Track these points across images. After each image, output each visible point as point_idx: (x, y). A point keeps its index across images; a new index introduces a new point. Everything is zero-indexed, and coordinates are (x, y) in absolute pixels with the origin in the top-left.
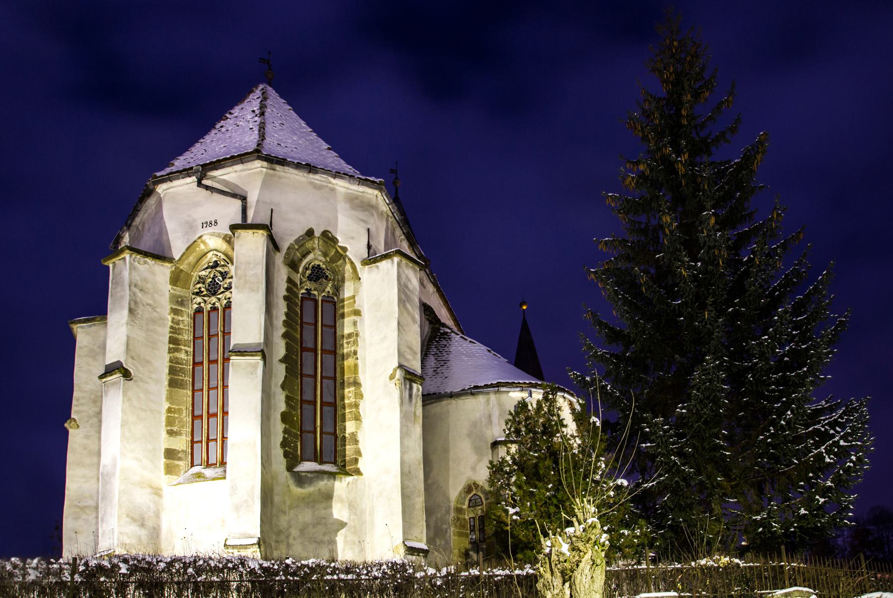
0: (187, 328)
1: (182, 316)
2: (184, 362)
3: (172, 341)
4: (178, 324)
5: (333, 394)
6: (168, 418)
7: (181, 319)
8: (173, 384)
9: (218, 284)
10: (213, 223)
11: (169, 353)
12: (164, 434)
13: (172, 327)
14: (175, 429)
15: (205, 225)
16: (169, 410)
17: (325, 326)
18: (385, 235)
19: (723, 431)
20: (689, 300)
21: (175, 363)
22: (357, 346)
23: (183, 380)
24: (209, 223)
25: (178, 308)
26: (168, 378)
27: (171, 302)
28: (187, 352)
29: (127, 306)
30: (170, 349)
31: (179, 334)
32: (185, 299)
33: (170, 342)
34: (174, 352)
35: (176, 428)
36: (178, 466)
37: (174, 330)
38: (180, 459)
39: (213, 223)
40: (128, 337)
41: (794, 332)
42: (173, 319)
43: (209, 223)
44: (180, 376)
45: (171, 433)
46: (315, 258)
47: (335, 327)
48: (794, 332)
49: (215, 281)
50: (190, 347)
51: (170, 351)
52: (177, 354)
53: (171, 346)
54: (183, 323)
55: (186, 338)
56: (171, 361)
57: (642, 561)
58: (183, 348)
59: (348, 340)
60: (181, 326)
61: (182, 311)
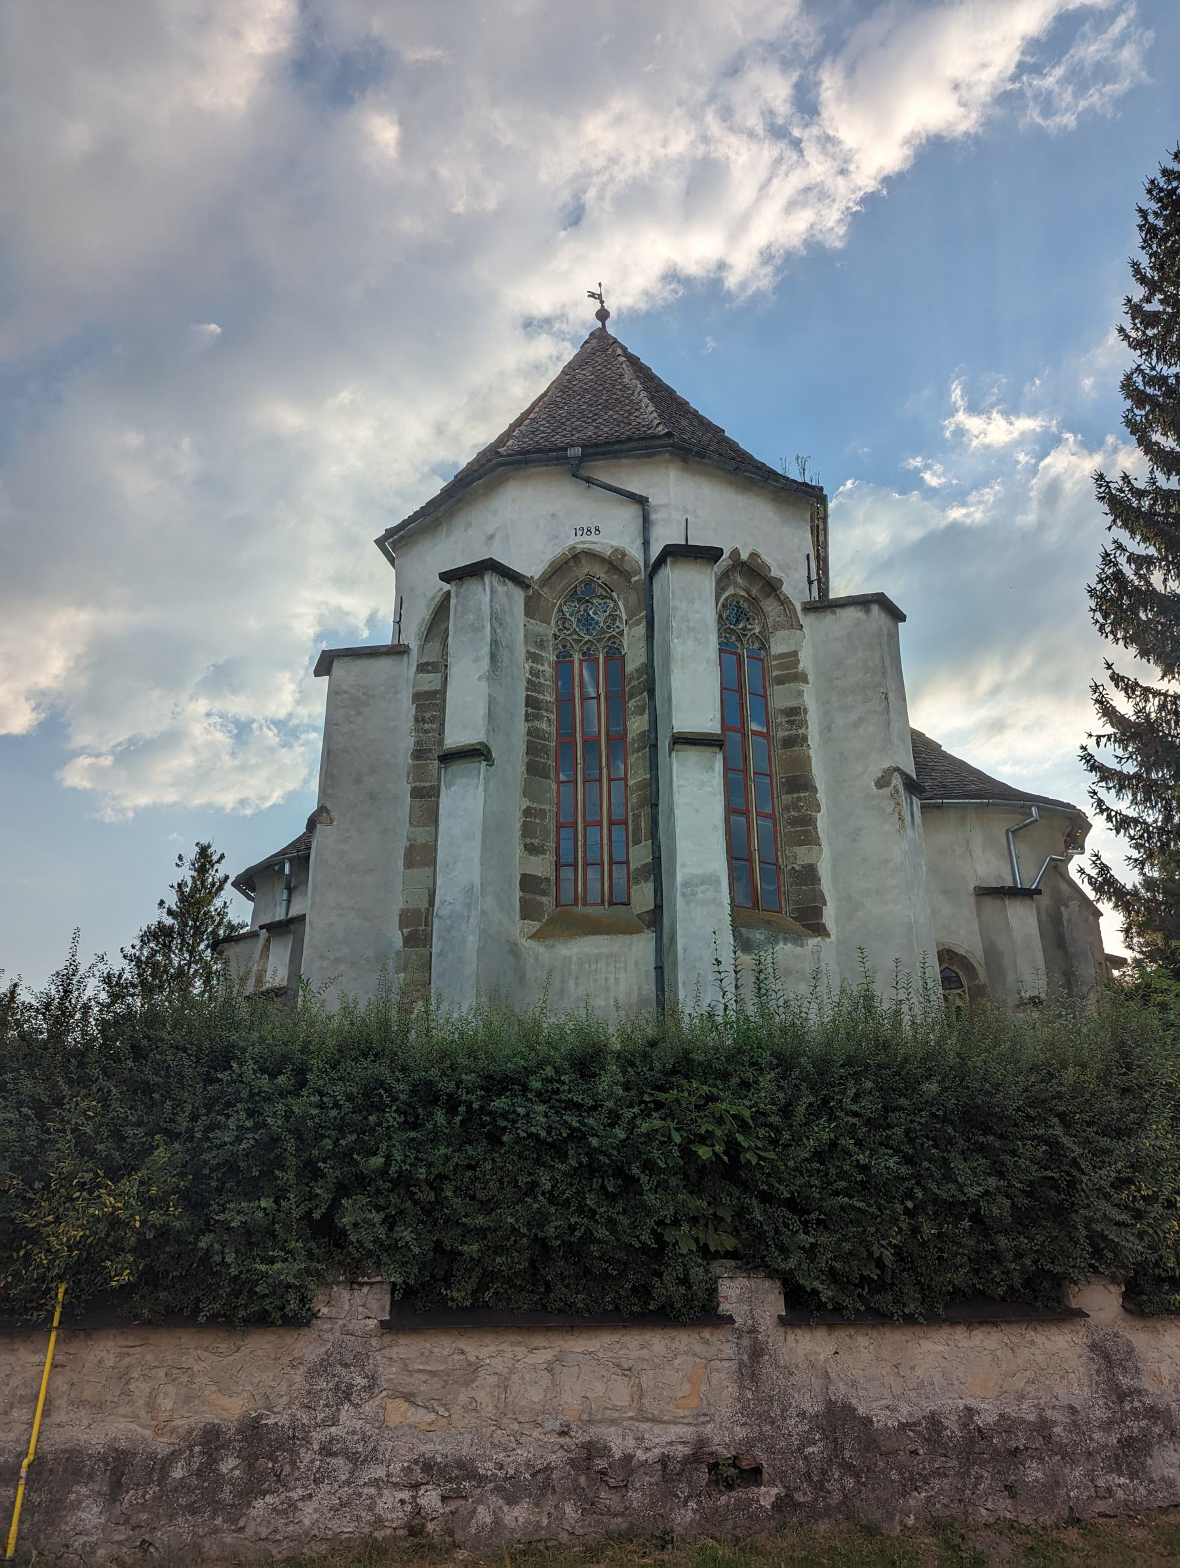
0: (548, 683)
1: (543, 665)
2: (547, 735)
3: (530, 702)
5: (1006, 852)
6: (525, 826)
7: (541, 668)
8: (534, 769)
9: (593, 619)
10: (593, 530)
11: (527, 720)
12: (518, 850)
13: (529, 681)
14: (536, 842)
15: (579, 533)
16: (527, 812)
18: (825, 546)
21: (534, 737)
22: (807, 728)
23: (546, 763)
24: (585, 530)
26: (526, 759)
28: (549, 720)
30: (527, 715)
32: (545, 639)
33: (527, 705)
34: (533, 721)
35: (537, 841)
36: (541, 904)
37: (532, 685)
38: (544, 893)
39: (593, 530)
40: (490, 696)
41: (1169, 244)
42: (531, 668)
43: (585, 530)
45: (531, 849)
47: (765, 696)
48: (1169, 244)
49: (588, 615)
50: (552, 712)
51: (527, 718)
52: (537, 724)
53: (530, 710)
54: (544, 675)
55: (548, 698)
56: (529, 733)
58: (545, 714)
59: (792, 718)
61: (542, 656)
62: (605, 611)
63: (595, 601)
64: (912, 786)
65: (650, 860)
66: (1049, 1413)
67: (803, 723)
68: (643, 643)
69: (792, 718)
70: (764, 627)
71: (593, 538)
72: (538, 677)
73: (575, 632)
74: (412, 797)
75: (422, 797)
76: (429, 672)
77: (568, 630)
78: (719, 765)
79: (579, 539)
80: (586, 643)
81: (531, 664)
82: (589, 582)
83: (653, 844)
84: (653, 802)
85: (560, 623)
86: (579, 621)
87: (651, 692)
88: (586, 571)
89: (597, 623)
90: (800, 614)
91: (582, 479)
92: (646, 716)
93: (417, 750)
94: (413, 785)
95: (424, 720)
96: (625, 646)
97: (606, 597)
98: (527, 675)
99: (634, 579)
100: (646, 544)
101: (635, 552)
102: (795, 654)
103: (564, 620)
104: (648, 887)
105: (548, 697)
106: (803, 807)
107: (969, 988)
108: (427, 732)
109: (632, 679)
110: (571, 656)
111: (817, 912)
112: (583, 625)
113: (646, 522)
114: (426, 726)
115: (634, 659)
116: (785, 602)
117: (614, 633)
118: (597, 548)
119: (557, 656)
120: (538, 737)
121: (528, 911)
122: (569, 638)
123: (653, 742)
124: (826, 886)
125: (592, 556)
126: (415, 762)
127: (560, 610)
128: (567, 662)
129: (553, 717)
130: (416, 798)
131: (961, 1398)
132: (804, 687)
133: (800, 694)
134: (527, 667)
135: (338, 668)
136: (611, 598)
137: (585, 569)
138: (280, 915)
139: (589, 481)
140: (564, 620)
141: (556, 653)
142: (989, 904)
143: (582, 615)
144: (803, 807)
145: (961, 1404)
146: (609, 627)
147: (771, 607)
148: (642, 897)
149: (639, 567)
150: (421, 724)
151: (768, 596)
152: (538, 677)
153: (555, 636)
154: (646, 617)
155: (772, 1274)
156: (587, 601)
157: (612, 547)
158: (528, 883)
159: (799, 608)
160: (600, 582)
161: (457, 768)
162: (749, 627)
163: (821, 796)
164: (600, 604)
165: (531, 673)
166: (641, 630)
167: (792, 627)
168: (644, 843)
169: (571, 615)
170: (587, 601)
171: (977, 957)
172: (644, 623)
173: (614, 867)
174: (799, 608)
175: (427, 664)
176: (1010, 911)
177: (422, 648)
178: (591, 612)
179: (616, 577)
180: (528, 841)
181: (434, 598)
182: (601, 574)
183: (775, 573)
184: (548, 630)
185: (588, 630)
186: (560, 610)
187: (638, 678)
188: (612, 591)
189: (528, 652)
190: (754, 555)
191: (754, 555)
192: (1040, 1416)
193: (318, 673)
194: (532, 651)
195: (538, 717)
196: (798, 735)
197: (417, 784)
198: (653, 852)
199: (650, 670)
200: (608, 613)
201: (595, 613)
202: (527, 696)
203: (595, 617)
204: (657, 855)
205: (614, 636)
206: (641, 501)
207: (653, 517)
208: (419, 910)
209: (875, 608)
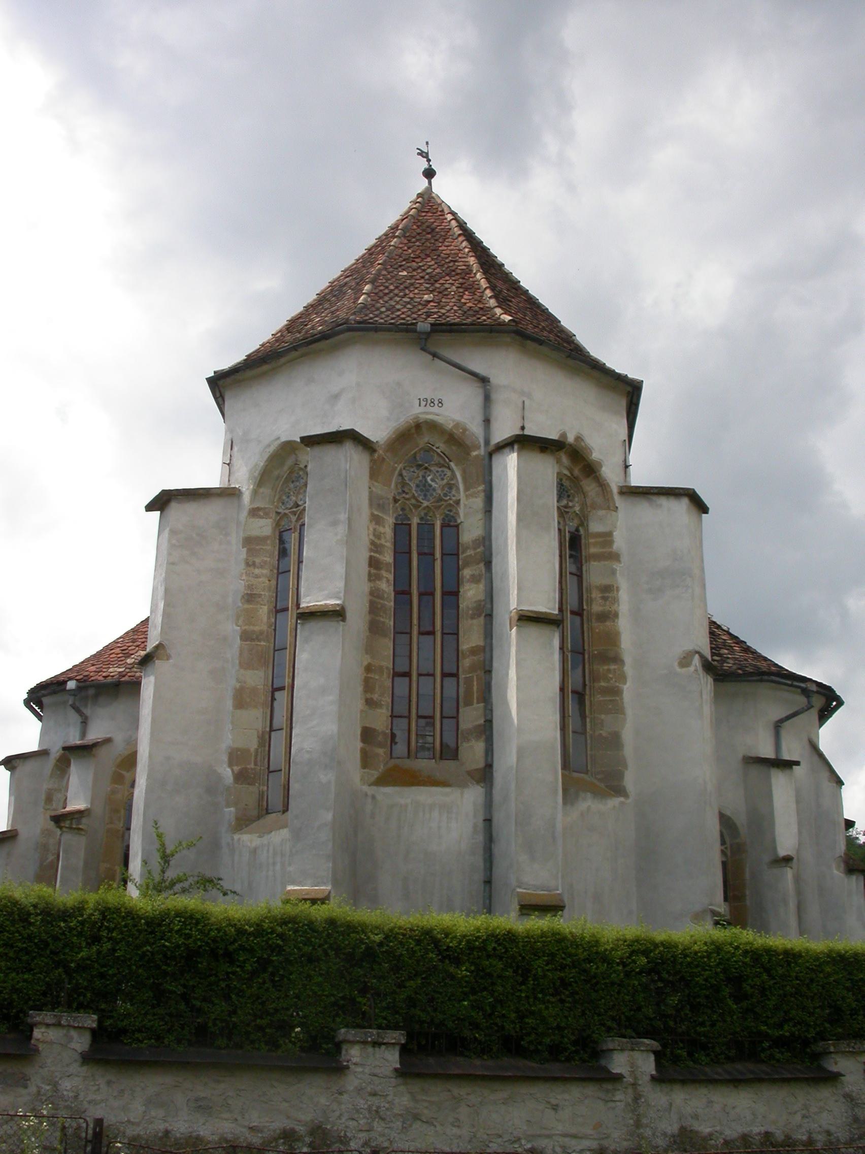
1: (384, 527)
4: (379, 538)
8: (375, 628)
9: (430, 486)
10: (436, 402)
11: (370, 580)
13: (372, 543)
15: (423, 403)
17: (407, 553)
19: (507, 318)
20: (568, 523)
24: (429, 402)
25: (380, 514)
27: (371, 505)
28: (388, 581)
29: (266, 506)
31: (380, 553)
34: (374, 580)
39: (436, 402)
42: (375, 530)
43: (429, 402)
44: (380, 616)
46: (571, 498)
49: (426, 481)
50: (391, 573)
54: (385, 538)
56: (372, 593)
57: (654, 1015)
60: (383, 541)
61: (383, 518)
62: (443, 479)
63: (432, 469)
64: (708, 667)
65: (482, 721)
66: (814, 1136)
67: (615, 600)
68: (480, 516)
69: (607, 595)
70: (584, 505)
71: (435, 409)
72: (379, 538)
73: (414, 497)
74: (241, 639)
75: (252, 640)
76: (261, 517)
77: (407, 493)
78: (556, 643)
79: (422, 409)
80: (424, 508)
81: (374, 526)
82: (428, 450)
83: (485, 708)
84: (487, 668)
85: (399, 486)
86: (417, 486)
87: (488, 564)
88: (426, 439)
89: (434, 490)
90: (616, 497)
91: (430, 353)
92: (481, 586)
93: (247, 594)
94: (244, 628)
95: (254, 564)
96: (462, 515)
97: (443, 466)
98: (371, 537)
99: (474, 453)
100: (487, 422)
101: (476, 428)
102: (609, 534)
103: (404, 484)
104: (479, 747)
105: (388, 557)
106: (612, 678)
107: (731, 846)
108: (257, 577)
109: (468, 548)
110: (409, 519)
111: (620, 776)
112: (422, 491)
113: (487, 399)
114: (257, 571)
115: (470, 531)
116: (603, 485)
117: (451, 502)
118: (439, 419)
119: (396, 519)
120: (379, 597)
121: (366, 760)
122: (407, 502)
123: (489, 612)
124: (628, 751)
125: (433, 427)
126: (246, 606)
127: (401, 475)
128: (405, 524)
129: (391, 577)
130: (246, 641)
131: (762, 1126)
132: (616, 566)
133: (613, 572)
134: (371, 529)
135: (175, 509)
136: (449, 468)
137: (425, 439)
138: (75, 739)
139: (435, 355)
140: (404, 484)
141: (395, 515)
142: (755, 771)
143: (420, 481)
144: (612, 678)
145: (763, 1129)
146: (446, 495)
147: (590, 487)
148: (473, 752)
149: (479, 443)
150: (251, 568)
151: (588, 476)
152: (379, 538)
153: (396, 501)
154: (484, 491)
155: (781, 954)
156: (426, 468)
157: (453, 421)
158: (367, 735)
159: (615, 490)
160: (439, 451)
161: (314, 625)
162: (570, 504)
163: (628, 669)
164: (437, 472)
165: (374, 535)
166: (478, 502)
167: (608, 508)
168: (475, 705)
169: (410, 480)
170: (426, 468)
171: (741, 820)
172: (482, 495)
173: (406, 714)
174: (615, 490)
175: (258, 509)
176: (774, 781)
177: (255, 493)
178: (429, 479)
179: (454, 448)
180: (369, 696)
181: (269, 446)
182: (441, 446)
183: (595, 456)
184: (388, 491)
185: (425, 495)
186: (401, 475)
187: (475, 549)
188: (450, 461)
189: (372, 515)
190: (579, 438)
191: (579, 438)
192: (810, 1138)
193: (150, 507)
194: (376, 513)
195: (379, 578)
196: (610, 611)
197: (246, 627)
198: (485, 716)
199: (487, 543)
200: (445, 481)
201: (432, 480)
202: (371, 557)
203: (433, 484)
204: (489, 718)
205: (450, 505)
206: (484, 381)
207: (494, 396)
208: (248, 751)
209: (685, 501)
